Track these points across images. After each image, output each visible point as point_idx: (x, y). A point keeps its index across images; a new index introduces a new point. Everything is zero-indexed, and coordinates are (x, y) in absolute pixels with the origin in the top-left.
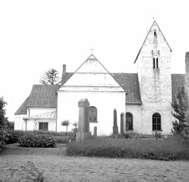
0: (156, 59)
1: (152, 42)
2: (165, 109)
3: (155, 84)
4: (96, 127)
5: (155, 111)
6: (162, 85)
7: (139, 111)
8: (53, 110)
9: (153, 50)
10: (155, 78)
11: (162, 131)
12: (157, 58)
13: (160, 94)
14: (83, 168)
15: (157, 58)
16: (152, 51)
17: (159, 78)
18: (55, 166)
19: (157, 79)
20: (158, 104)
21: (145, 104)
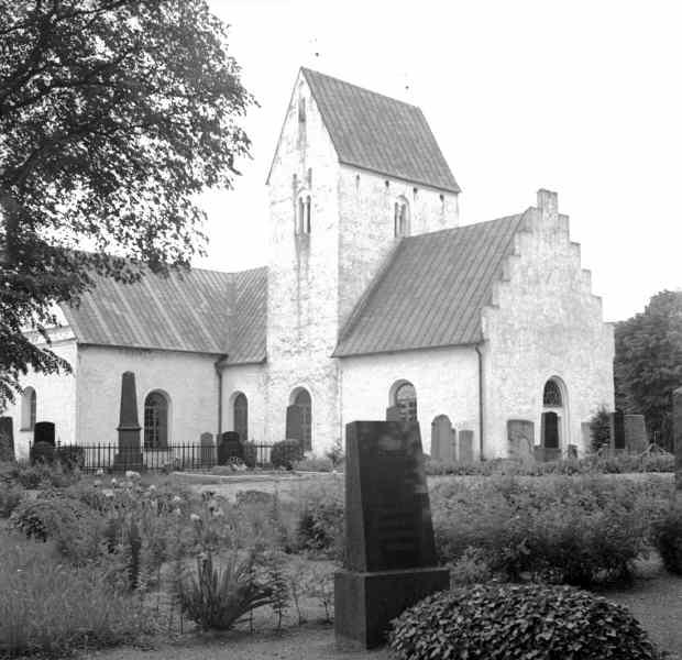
0: (305, 201)
1: (295, 144)
2: (320, 374)
3: (299, 288)
4: (302, 68)
5: (295, 384)
6: (315, 290)
7: (260, 385)
8: (38, 420)
9: (296, 172)
10: (298, 269)
11: (498, 307)
12: (309, 198)
13: (309, 323)
14: (663, 622)
15: (309, 198)
16: (295, 176)
17: (307, 268)
18: (307, 546)
19: (303, 272)
20: (304, 357)
21: (277, 363)
